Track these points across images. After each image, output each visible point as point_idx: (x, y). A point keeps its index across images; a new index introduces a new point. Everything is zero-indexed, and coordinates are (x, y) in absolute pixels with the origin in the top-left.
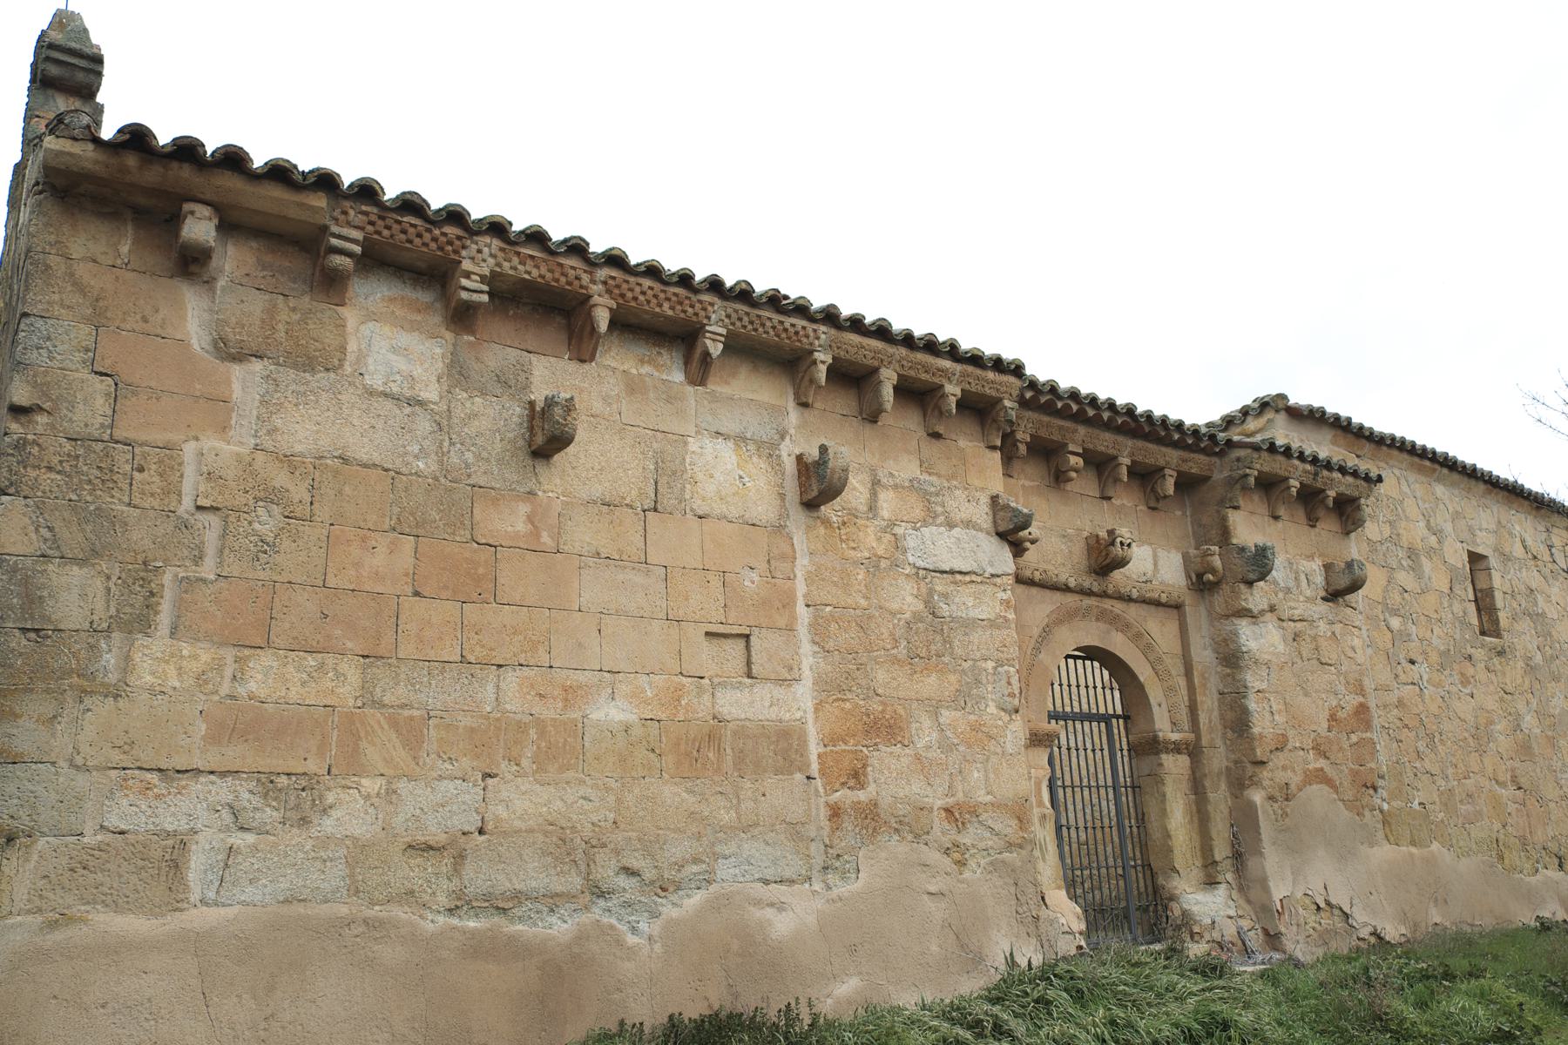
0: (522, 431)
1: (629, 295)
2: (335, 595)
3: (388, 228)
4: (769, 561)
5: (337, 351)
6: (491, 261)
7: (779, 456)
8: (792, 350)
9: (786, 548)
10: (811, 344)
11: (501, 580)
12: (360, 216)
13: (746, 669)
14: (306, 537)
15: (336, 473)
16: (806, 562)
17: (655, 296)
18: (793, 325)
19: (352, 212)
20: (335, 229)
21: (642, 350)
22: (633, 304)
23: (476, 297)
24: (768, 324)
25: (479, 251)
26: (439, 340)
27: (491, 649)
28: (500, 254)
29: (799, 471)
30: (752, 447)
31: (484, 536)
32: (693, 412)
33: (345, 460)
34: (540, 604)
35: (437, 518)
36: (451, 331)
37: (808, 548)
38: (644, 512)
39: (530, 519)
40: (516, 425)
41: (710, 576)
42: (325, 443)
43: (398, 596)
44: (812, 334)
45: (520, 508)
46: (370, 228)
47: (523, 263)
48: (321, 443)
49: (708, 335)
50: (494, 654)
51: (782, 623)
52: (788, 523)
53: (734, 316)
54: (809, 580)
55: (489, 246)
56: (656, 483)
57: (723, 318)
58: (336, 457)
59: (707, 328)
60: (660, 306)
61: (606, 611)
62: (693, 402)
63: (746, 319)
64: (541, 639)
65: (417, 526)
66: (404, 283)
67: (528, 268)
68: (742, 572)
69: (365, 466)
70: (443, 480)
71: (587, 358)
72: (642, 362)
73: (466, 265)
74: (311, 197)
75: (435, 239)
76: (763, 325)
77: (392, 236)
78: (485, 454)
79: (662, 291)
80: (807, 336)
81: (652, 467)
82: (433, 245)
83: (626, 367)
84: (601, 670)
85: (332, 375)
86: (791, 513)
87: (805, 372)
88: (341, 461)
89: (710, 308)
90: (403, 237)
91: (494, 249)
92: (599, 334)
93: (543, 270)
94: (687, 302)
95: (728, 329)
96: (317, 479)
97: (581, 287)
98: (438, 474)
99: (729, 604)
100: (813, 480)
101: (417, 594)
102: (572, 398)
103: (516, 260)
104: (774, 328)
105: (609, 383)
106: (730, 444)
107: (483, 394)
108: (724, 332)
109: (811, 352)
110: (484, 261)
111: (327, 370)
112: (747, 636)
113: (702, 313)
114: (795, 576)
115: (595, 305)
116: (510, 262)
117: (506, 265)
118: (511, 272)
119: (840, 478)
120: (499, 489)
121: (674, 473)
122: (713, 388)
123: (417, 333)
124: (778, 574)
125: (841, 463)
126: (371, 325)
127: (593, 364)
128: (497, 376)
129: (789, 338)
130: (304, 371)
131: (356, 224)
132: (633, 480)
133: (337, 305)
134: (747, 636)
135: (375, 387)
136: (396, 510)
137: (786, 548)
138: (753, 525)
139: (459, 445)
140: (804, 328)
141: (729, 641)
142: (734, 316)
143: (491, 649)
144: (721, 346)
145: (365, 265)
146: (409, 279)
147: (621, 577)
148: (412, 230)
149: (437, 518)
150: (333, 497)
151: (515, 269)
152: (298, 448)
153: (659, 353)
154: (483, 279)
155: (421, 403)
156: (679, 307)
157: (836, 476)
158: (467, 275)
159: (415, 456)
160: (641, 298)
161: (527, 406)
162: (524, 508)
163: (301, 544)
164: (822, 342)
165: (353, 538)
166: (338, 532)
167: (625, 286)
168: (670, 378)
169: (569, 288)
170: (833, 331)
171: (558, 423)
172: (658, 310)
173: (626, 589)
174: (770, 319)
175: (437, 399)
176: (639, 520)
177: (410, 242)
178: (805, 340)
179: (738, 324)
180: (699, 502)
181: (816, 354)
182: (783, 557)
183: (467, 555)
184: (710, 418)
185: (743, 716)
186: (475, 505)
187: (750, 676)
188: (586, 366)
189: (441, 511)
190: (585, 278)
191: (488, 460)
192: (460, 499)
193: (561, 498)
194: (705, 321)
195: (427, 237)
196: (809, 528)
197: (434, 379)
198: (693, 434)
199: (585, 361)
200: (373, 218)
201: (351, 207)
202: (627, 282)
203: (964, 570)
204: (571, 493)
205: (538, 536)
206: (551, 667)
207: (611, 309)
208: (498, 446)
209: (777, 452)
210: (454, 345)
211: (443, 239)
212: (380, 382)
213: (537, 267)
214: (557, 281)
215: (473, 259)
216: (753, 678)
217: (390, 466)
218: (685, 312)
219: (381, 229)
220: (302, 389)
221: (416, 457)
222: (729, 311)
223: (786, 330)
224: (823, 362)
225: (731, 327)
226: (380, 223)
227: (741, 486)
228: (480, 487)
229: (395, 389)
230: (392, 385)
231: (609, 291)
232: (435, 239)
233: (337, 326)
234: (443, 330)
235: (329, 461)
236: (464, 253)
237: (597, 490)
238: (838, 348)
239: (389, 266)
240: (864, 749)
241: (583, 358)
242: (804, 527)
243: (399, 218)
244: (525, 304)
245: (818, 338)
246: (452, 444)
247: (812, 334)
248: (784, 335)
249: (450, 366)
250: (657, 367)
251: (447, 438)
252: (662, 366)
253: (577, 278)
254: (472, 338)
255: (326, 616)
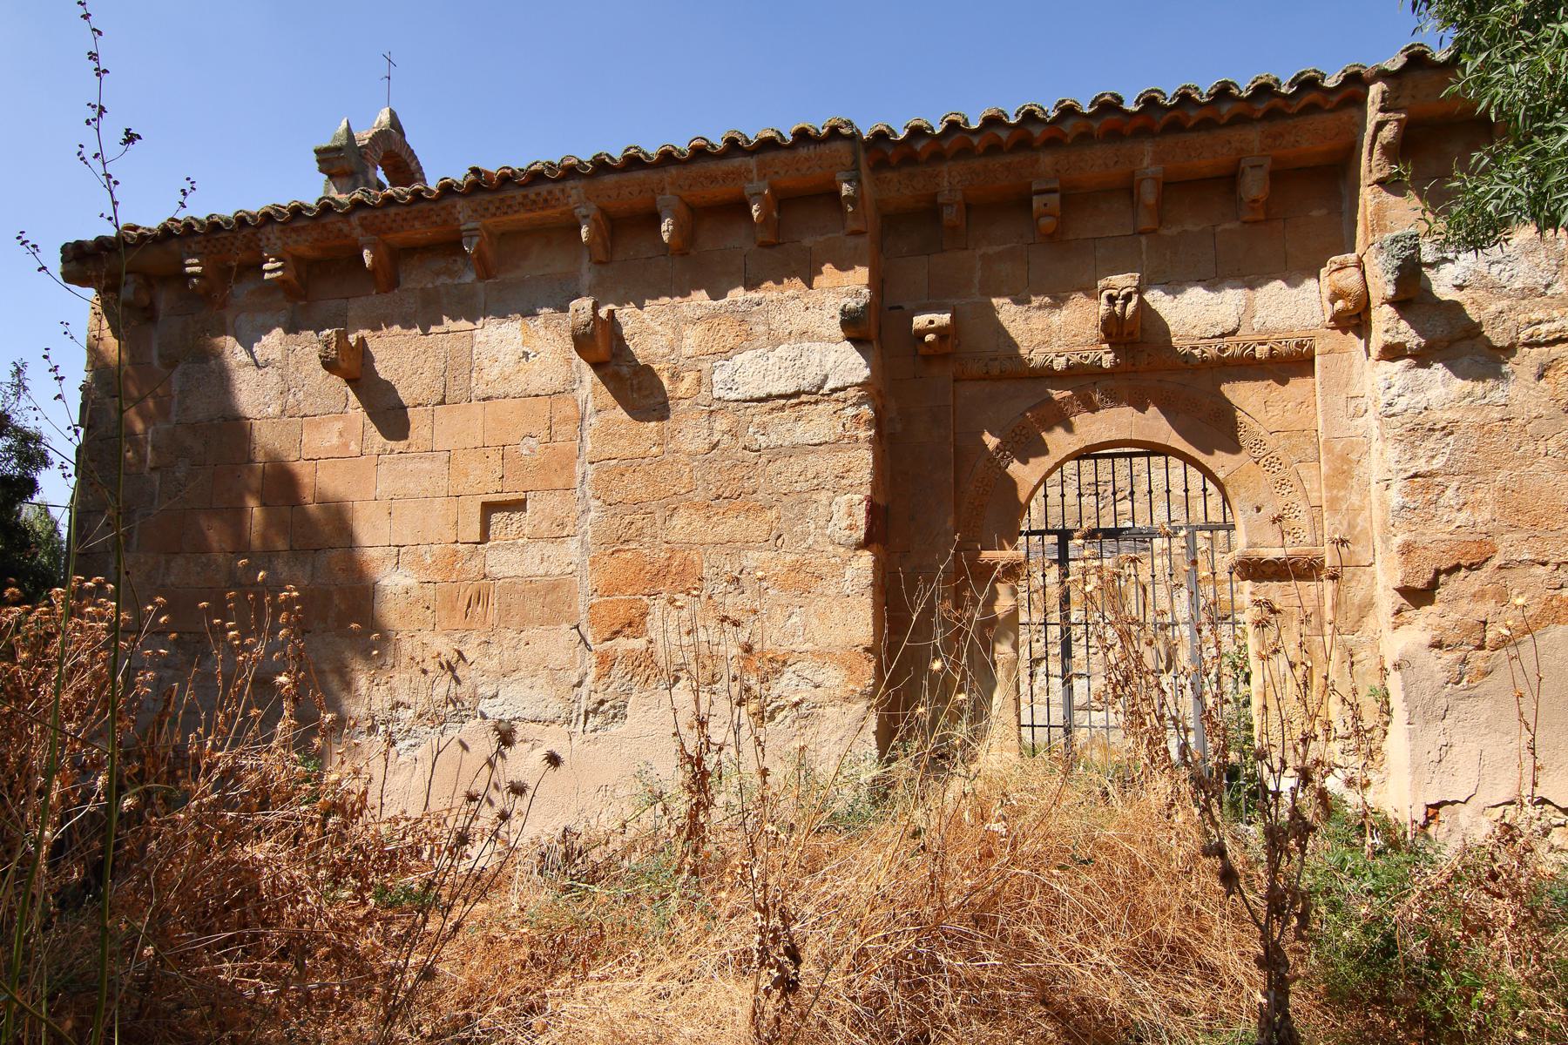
4: (550, 428)
33: (226, 420)
41: (489, 452)
59: (462, 228)
140: (550, 192)
147: (410, 467)
152: (200, 416)
185: (512, 574)
203: (789, 392)
240: (645, 598)
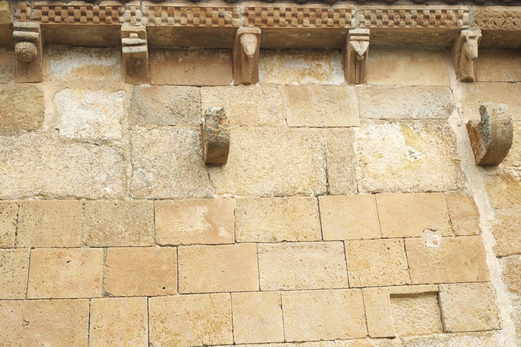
0: (196, 148)
1: (270, 19)
2: (35, 305)
3: (58, 14)
5: (37, 115)
6: (145, 20)
7: (448, 128)
8: (441, 35)
9: (466, 207)
10: (456, 24)
11: (182, 274)
12: (35, 10)
13: (440, 324)
14: (11, 261)
15: (36, 207)
16: (491, 216)
17: (294, 15)
18: (432, 12)
19: (29, 10)
20: (17, 24)
21: (302, 65)
22: (276, 26)
23: (135, 49)
24: (408, 16)
25: (133, 14)
26: (120, 92)
27: (177, 334)
28: (151, 13)
29: (470, 137)
30: (419, 125)
31: (165, 238)
32: (356, 106)
33: (43, 196)
34: (221, 290)
35: (124, 230)
36: (130, 83)
37: (492, 204)
38: (317, 196)
39: (207, 218)
40: (190, 144)
41: (389, 243)
42: (27, 186)
43: (90, 299)
44: (454, 15)
45: (198, 211)
46: (45, 18)
47: (171, 15)
48: (24, 186)
49: (352, 37)
50: (179, 338)
51: (472, 276)
52: (466, 185)
53: (373, 16)
54: (497, 232)
55: (140, 8)
56: (326, 170)
57: (363, 20)
58: (37, 195)
59: (351, 32)
60: (302, 22)
61: (285, 288)
62: (355, 99)
63: (385, 16)
64: (224, 320)
65: (106, 239)
66: (91, 56)
67: (177, 17)
68: (423, 235)
69: (60, 198)
70: (127, 199)
71: (249, 80)
72: (303, 75)
73: (125, 27)
74: (276, 71)
75: (96, 14)
76: (403, 18)
77: (63, 19)
78: (163, 173)
79: (300, 10)
80: (450, 18)
81: (321, 158)
82: (96, 19)
83: (287, 82)
84: (285, 342)
85: (33, 134)
86: (468, 176)
87: (460, 51)
88: (41, 197)
89: (348, 14)
90: (71, 18)
91: (145, 9)
92: (247, 58)
93: (190, 17)
94: (325, 14)
95: (371, 29)
96: (21, 215)
97: (226, 22)
98: (122, 194)
99: (412, 266)
100: (481, 140)
101: (107, 295)
102: (222, 110)
103: (165, 14)
104: (414, 18)
105: (273, 97)
106: (397, 126)
107: (159, 125)
108: (368, 31)
109: (459, 32)
110: (139, 20)
111: (30, 131)
112: (437, 294)
113: (342, 20)
114: (480, 231)
115: (242, 34)
116: (161, 16)
117: (158, 20)
118: (164, 24)
119: (503, 132)
120: (178, 198)
121: (343, 159)
122: (374, 83)
123: (101, 91)
124: (462, 232)
125: (501, 118)
126: (64, 92)
127: (257, 85)
128: (171, 109)
129: (433, 24)
130: (11, 135)
131: (34, 17)
132: (304, 172)
133: (36, 82)
134: (437, 294)
135: (68, 136)
136: (87, 228)
137: (466, 207)
138: (430, 192)
139: (140, 169)
140: (444, 11)
141: (419, 300)
142: (373, 16)
143: (177, 334)
144: (366, 44)
145: (58, 50)
146: (95, 53)
147: (298, 255)
148: (76, 11)
149: (124, 230)
150: (34, 226)
151: (166, 21)
153: (318, 65)
154: (140, 35)
155: (106, 142)
156: (318, 20)
157: (499, 130)
158: (127, 34)
159: (103, 184)
160: (282, 19)
161: (199, 128)
162: (201, 210)
163: (6, 267)
164: (466, 20)
165: (50, 256)
166: (38, 254)
167: (264, 13)
168: (330, 83)
169: (216, 26)
170: (475, 8)
171: (211, 131)
172: (300, 26)
173: (305, 266)
174: (409, 11)
175: (120, 136)
176: (313, 204)
177: (78, 20)
178: (448, 22)
179: (379, 22)
180: (371, 180)
181: (464, 33)
182: (465, 216)
183: (151, 256)
184: (374, 109)
186: (156, 214)
187: (444, 331)
188: (251, 88)
189: (126, 223)
190: (228, 15)
191: (166, 177)
192: (144, 211)
193: (236, 196)
194: (347, 26)
195: (90, 13)
196: (489, 186)
197: (116, 121)
198: (358, 124)
199: (250, 84)
200: (45, 9)
201: (28, 6)
202: (266, 9)
204: (245, 191)
205: (215, 230)
206: (234, 344)
207: (257, 35)
208: (175, 164)
209: (446, 125)
210: (133, 93)
211: (103, 12)
212: (72, 133)
213: (183, 15)
214: (204, 22)
215: (129, 21)
216: (447, 332)
217: (82, 195)
218: (326, 22)
219: (53, 16)
220: (8, 149)
221: (104, 184)
222: (367, 12)
223: (427, 17)
224: (472, 38)
225: (373, 26)
226: (51, 11)
227: (412, 160)
228: (161, 199)
229: (84, 135)
230: (82, 132)
231: (251, 21)
232: (96, 14)
233: (36, 98)
234: (123, 85)
235: (31, 199)
236: (121, 19)
237: (269, 186)
238: (485, 22)
239: (78, 46)
241: (246, 81)
242: (483, 185)
243: (65, 4)
244: (192, 51)
245: (461, 17)
246: (134, 169)
247: (454, 15)
248: (426, 22)
249: (130, 110)
250: (318, 76)
251: (130, 165)
252: (322, 74)
253: (221, 16)
254: (148, 85)
255: (28, 323)
